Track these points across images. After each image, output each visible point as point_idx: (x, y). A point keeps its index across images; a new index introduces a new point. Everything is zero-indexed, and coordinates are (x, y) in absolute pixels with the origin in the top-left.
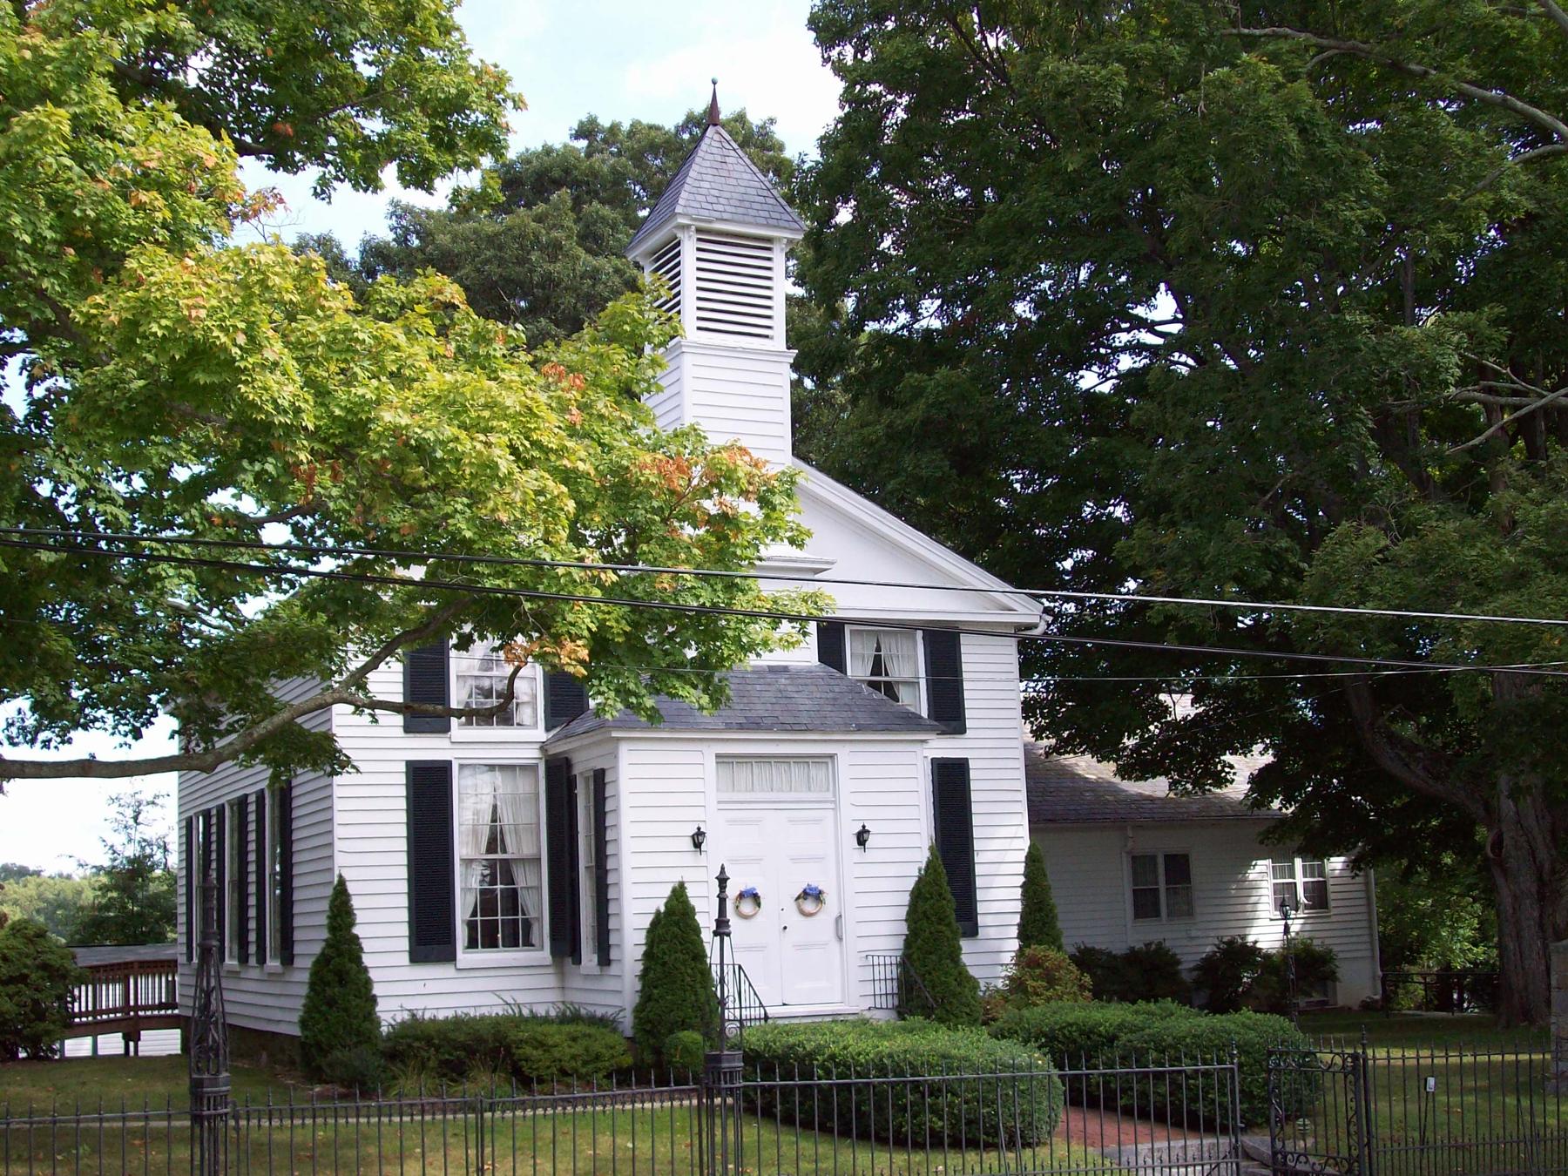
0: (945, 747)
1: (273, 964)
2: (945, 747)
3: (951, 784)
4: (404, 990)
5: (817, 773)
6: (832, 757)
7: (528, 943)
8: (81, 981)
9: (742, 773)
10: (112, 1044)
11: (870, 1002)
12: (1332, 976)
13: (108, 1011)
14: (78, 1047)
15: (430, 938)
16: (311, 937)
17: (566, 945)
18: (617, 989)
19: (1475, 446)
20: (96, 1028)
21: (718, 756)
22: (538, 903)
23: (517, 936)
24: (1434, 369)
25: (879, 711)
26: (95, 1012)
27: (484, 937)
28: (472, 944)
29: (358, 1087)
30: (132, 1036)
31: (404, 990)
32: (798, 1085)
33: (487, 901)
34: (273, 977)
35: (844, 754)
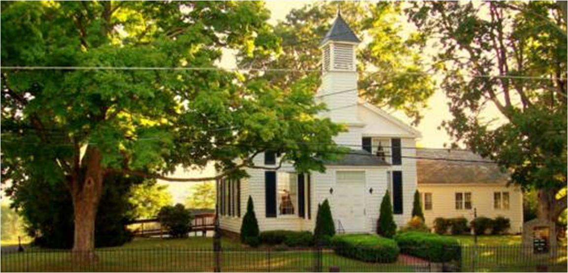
0: (396, 168)
1: (236, 217)
2: (396, 168)
3: (397, 178)
4: (266, 224)
5: (359, 175)
6: (364, 172)
7: (293, 213)
8: (193, 219)
9: (342, 176)
10: (200, 234)
11: (371, 229)
12: (509, 226)
13: (199, 226)
14: (191, 234)
15: (271, 211)
16: (244, 210)
17: (302, 214)
18: (309, 225)
19: (21, 66)
20: (196, 230)
21: (338, 172)
22: (296, 206)
23: (292, 211)
24: (425, 78)
25: (379, 160)
26: (196, 226)
27: (284, 212)
28: (281, 214)
29: (254, 245)
30: (204, 231)
31: (266, 224)
32: (347, 249)
33: (284, 204)
34: (236, 219)
35: (366, 170)
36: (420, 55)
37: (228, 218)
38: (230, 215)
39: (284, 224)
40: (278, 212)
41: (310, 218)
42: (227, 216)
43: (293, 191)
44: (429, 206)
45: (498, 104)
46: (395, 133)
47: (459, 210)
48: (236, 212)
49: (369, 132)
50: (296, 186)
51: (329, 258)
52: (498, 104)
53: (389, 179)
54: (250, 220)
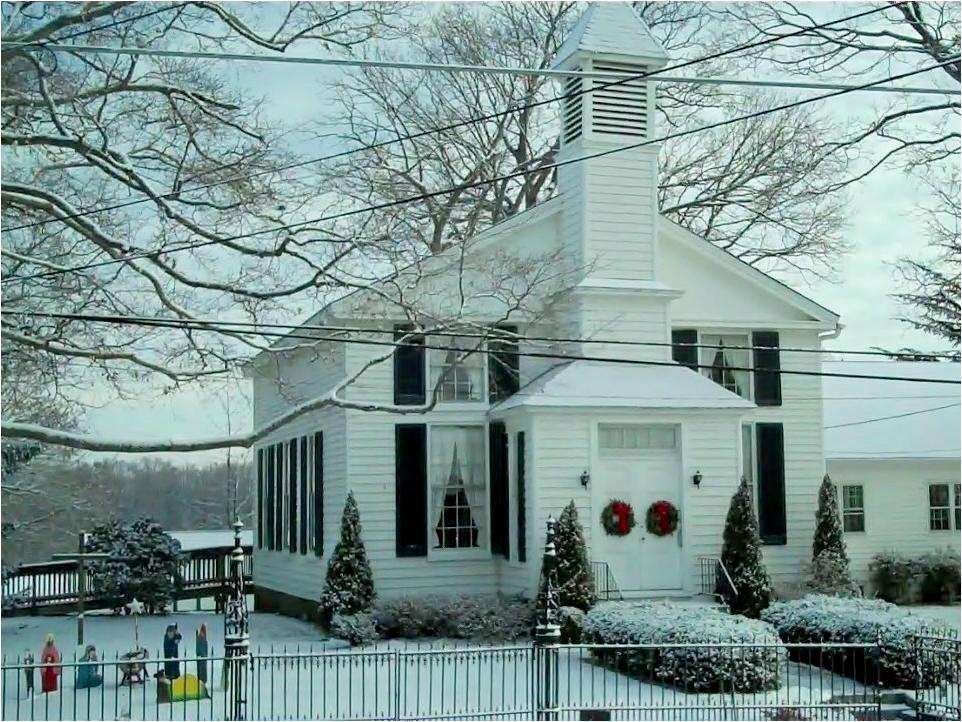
0: (768, 415)
1: (311, 555)
4: (396, 579)
15: (411, 540)
16: (333, 537)
22: (482, 518)
23: (468, 539)
31: (396, 579)
33: (449, 516)
36: (140, 270)
37: (287, 560)
38: (293, 549)
39: (468, 585)
40: (432, 539)
41: (522, 558)
42: (286, 552)
43: (477, 481)
44: (857, 524)
45: (554, 303)
46: (766, 321)
47: (941, 533)
48: (311, 540)
49: (685, 315)
50: (432, 466)
51: (583, 686)
52: (554, 303)
53: (747, 443)
54: (349, 568)
